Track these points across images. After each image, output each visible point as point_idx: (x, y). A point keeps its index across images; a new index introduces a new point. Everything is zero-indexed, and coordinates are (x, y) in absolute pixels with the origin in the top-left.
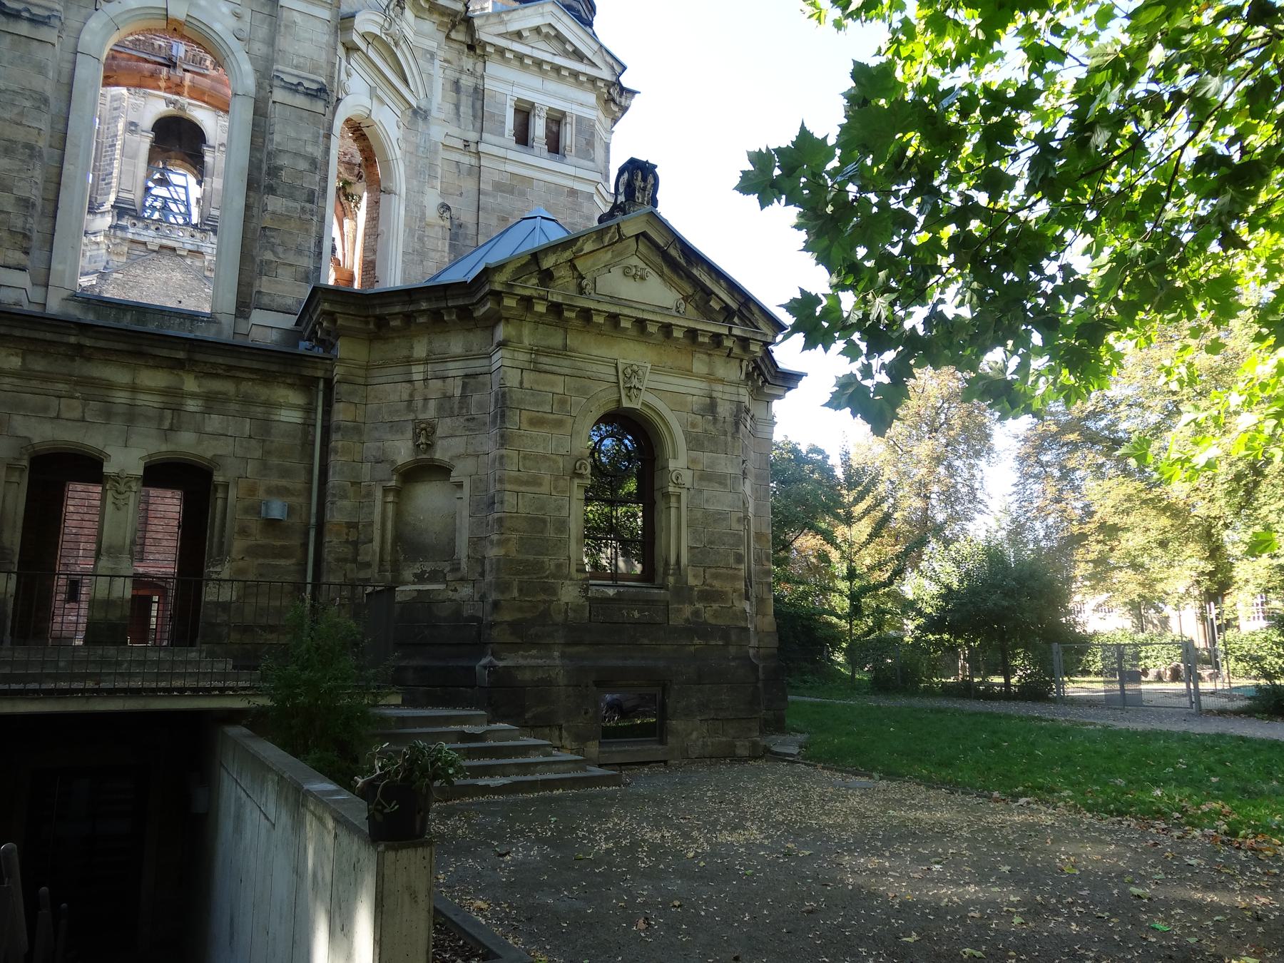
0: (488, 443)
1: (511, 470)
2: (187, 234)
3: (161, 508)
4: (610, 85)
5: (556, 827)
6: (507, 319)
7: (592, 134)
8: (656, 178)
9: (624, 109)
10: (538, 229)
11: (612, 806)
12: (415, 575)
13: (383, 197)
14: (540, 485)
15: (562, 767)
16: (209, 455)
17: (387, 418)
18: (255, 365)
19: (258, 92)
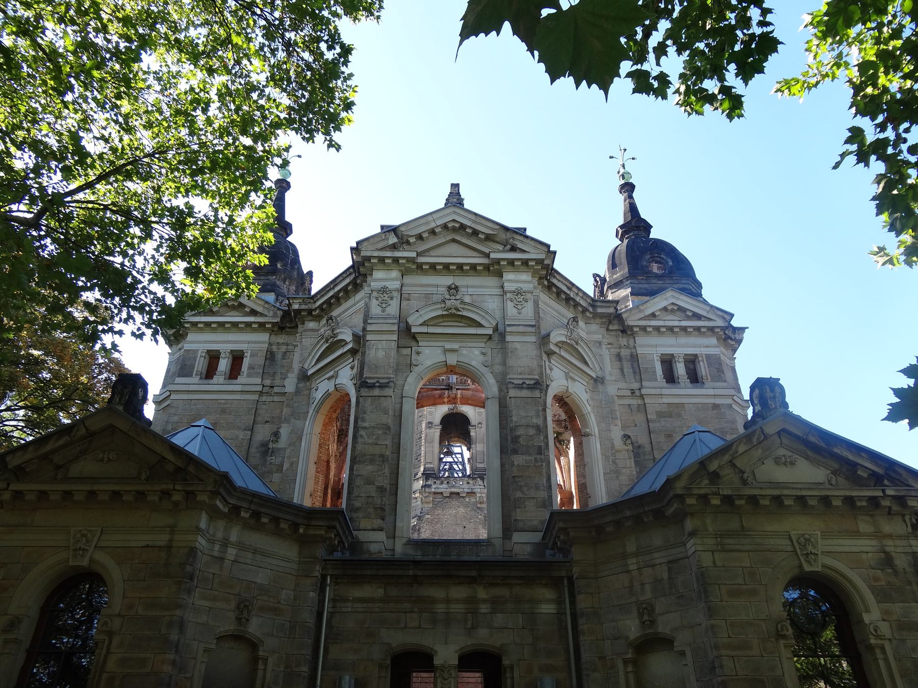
4: (723, 329)
6: (691, 514)
7: (720, 364)
9: (739, 342)
10: (698, 441)
13: (584, 439)
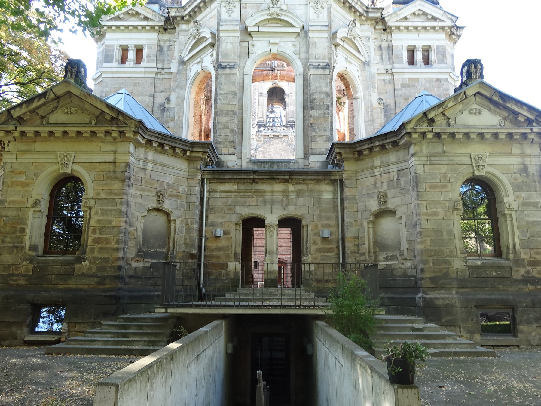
0: (411, 199)
1: (423, 210)
2: (282, 129)
3: (282, 232)
4: (450, 27)
5: (465, 376)
6: (415, 143)
7: (445, 52)
8: (482, 66)
9: (459, 36)
10: (424, 100)
11: (493, 367)
12: (384, 258)
13: (354, 101)
14: (438, 215)
15: (463, 346)
16: (300, 214)
17: (366, 192)
18: (313, 177)
19: (304, 72)
